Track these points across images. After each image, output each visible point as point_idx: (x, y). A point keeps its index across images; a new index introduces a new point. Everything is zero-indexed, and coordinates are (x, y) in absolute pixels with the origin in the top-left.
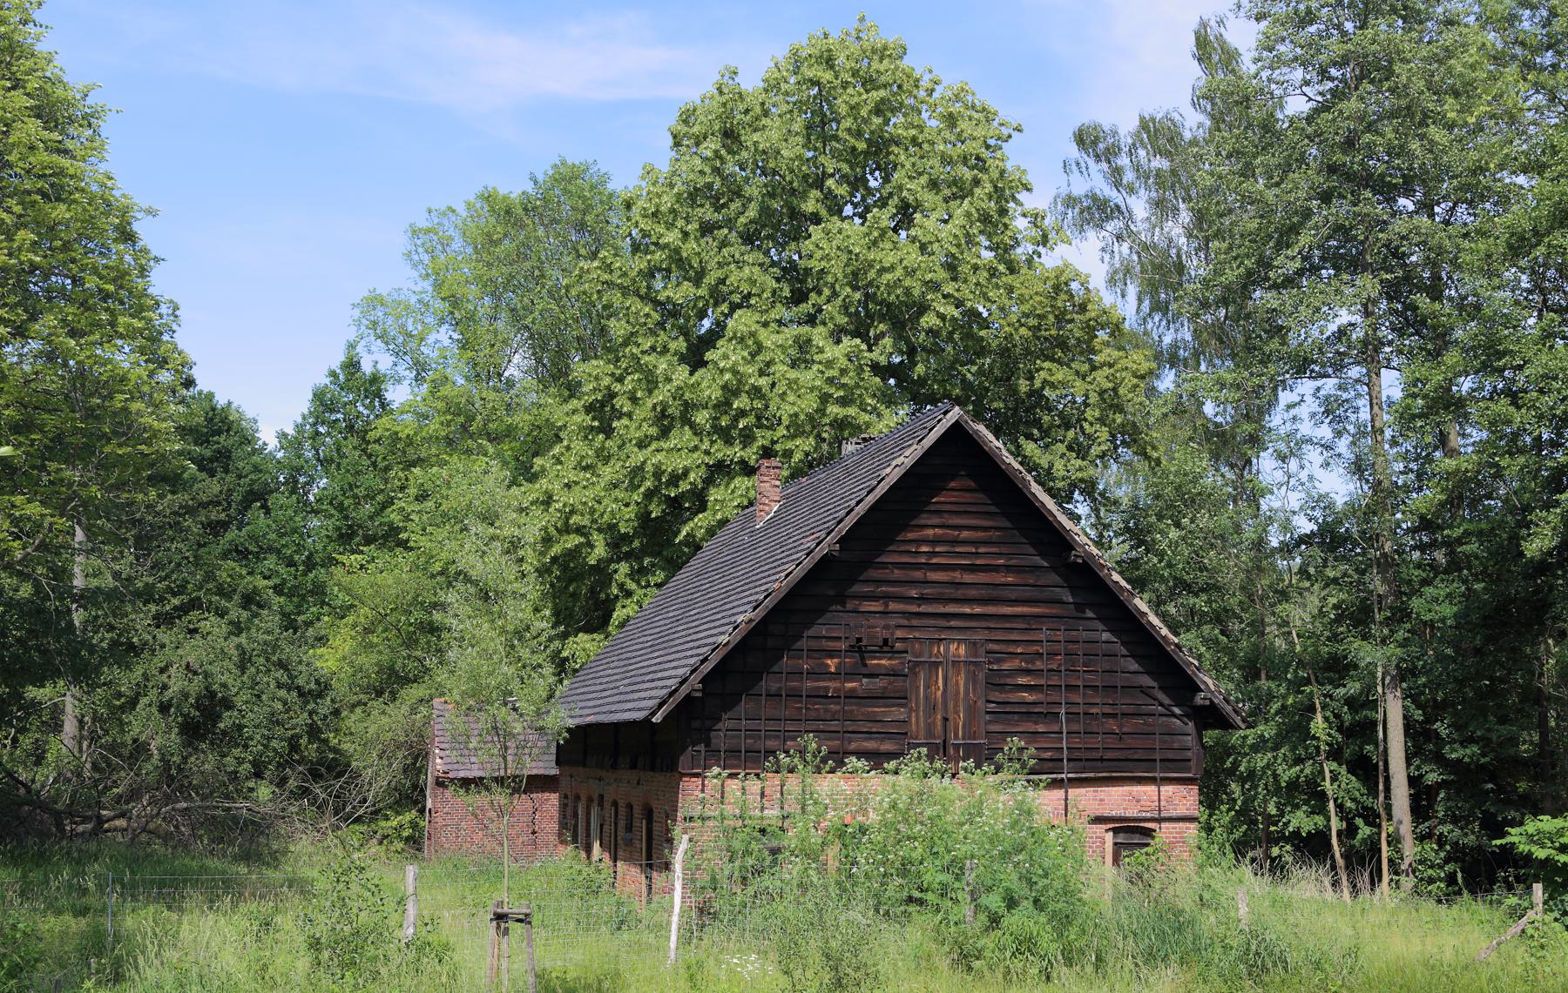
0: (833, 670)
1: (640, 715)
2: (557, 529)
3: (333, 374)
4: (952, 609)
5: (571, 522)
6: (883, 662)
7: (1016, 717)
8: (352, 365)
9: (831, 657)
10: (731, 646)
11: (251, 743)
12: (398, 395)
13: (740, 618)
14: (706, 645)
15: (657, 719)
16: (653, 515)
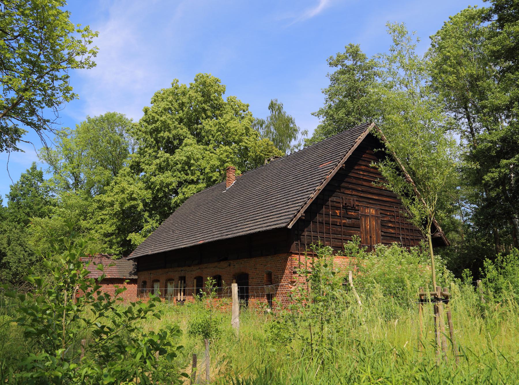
0: (338, 215)
1: (284, 225)
2: (127, 199)
3: (28, 171)
4: (370, 196)
5: (133, 196)
6: (352, 213)
7: (389, 238)
8: (34, 168)
9: (337, 210)
10: (314, 199)
11: (12, 268)
12: (47, 177)
13: (317, 188)
14: (306, 198)
15: (290, 227)
16: (159, 196)
